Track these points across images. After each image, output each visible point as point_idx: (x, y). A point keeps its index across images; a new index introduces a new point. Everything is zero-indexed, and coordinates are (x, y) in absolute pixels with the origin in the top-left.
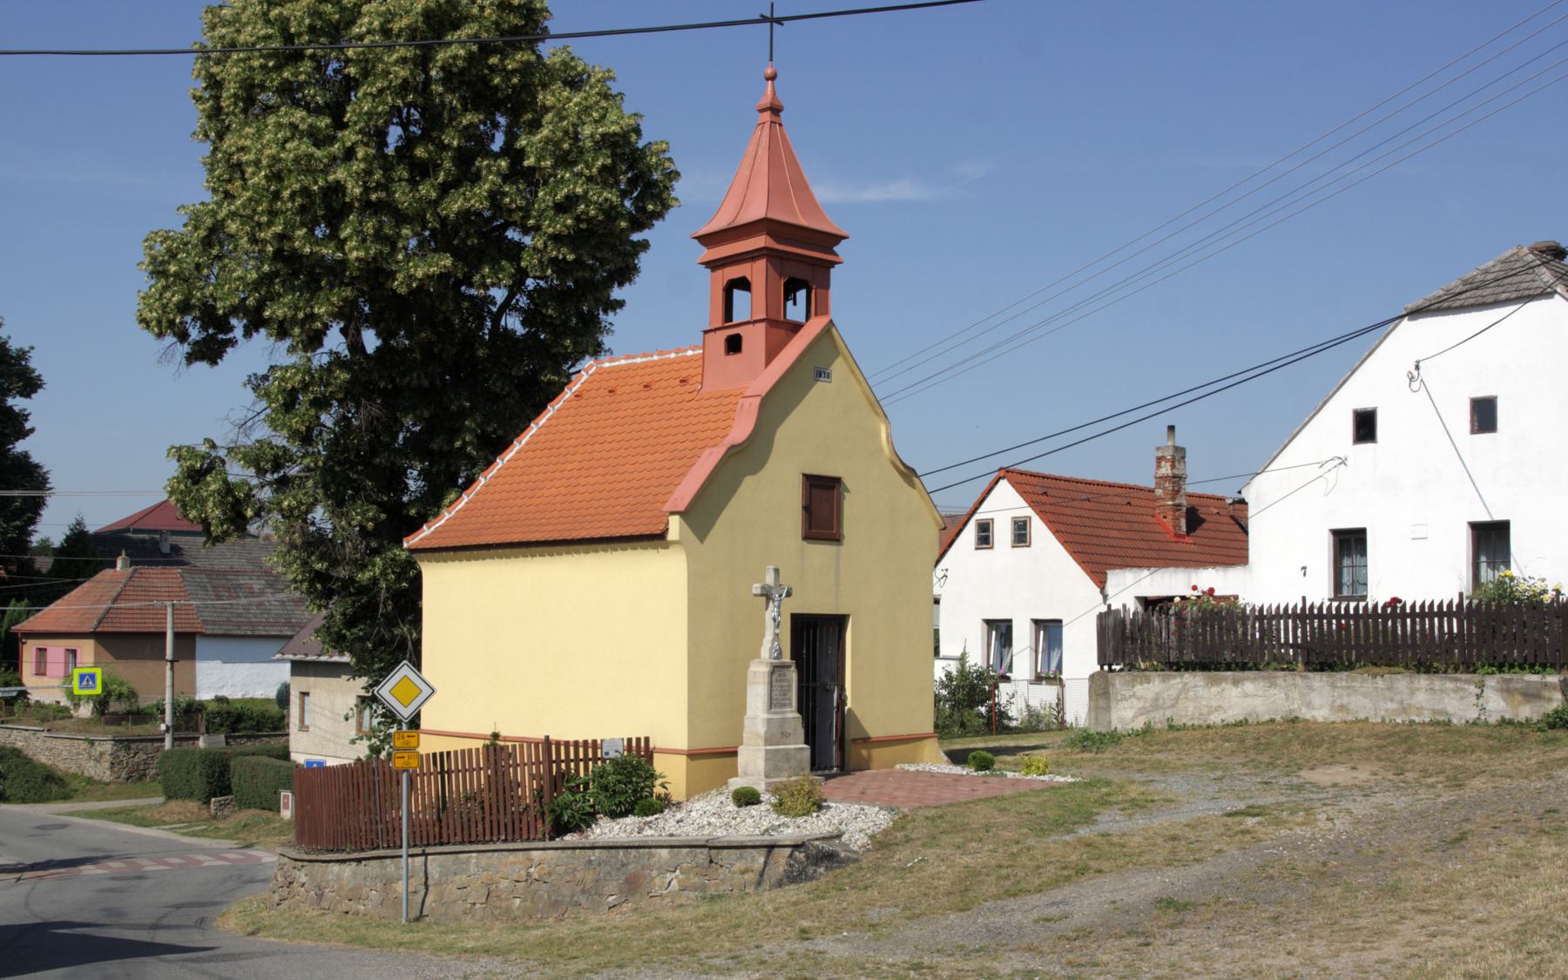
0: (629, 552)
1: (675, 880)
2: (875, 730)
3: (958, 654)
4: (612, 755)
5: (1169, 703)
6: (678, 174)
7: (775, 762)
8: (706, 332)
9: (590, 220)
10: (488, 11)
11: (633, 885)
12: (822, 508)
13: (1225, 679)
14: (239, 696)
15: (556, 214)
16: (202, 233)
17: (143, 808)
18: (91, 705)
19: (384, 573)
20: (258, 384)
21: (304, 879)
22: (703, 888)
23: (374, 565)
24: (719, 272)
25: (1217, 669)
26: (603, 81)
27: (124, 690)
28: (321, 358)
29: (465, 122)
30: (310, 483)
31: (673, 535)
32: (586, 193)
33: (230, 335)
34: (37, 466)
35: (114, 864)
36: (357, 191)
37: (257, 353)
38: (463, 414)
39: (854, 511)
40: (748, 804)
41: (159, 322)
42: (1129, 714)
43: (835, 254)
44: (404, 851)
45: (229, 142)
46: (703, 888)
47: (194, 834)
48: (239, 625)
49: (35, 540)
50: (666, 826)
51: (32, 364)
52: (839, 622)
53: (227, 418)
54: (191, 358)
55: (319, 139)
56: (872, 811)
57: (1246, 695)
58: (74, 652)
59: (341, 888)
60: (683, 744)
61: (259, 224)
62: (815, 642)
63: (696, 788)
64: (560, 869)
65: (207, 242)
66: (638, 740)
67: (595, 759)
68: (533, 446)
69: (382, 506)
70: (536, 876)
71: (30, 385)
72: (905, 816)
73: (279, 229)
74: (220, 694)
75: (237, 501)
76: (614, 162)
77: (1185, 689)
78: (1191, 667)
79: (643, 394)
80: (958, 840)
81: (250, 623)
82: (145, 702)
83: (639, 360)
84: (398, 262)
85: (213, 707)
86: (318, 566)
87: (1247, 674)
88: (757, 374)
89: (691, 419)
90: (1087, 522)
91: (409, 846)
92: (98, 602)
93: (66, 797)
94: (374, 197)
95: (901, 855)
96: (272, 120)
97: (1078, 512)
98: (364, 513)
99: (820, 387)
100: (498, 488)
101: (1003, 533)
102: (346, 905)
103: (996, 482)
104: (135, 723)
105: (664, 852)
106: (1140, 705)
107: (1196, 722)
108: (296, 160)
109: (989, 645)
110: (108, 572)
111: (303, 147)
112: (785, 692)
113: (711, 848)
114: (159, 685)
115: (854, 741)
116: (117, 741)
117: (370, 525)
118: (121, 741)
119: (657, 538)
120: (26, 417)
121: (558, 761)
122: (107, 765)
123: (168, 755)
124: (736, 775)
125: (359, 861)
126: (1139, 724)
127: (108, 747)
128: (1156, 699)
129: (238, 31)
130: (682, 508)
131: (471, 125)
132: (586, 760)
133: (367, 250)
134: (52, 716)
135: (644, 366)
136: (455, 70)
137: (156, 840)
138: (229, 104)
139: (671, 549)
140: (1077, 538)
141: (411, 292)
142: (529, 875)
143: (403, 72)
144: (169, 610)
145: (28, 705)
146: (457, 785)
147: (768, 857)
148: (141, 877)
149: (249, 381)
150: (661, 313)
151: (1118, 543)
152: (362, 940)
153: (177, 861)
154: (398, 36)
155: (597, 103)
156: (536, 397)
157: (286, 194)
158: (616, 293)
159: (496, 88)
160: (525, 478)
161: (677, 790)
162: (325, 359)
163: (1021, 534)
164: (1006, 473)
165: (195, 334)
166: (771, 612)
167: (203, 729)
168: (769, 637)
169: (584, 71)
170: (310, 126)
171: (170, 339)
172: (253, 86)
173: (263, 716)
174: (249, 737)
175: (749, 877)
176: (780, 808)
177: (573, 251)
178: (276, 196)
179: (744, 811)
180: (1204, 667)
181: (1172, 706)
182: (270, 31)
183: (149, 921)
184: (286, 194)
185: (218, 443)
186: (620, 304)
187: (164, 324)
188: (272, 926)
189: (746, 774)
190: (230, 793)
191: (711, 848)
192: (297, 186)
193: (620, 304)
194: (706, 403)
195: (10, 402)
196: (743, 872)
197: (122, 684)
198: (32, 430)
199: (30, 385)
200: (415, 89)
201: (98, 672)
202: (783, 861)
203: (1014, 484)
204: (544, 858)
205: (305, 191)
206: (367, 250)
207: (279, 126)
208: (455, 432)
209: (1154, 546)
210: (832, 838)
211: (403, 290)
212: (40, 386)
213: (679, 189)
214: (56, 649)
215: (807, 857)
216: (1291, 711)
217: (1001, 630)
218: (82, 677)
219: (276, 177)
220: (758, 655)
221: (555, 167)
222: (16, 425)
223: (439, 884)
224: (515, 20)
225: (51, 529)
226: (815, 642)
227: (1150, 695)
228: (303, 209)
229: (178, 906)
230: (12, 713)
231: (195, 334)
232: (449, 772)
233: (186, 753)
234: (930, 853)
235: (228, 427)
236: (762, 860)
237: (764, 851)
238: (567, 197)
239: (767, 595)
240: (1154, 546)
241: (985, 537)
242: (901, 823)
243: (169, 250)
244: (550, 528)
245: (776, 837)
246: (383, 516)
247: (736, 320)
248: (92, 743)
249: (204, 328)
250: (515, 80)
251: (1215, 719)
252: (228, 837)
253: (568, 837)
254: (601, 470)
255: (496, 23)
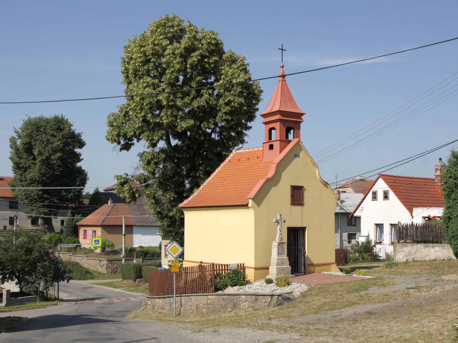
0: (239, 209)
1: (246, 304)
2: (315, 261)
3: (367, 235)
4: (233, 268)
5: (413, 253)
6: (262, 91)
7: (279, 271)
8: (264, 143)
9: (235, 107)
10: (204, 46)
11: (235, 306)
12: (297, 195)
13: (430, 246)
14: (147, 246)
15: (225, 106)
16: (124, 113)
17: (116, 282)
18: (100, 249)
19: (176, 213)
20: (141, 155)
21: (150, 303)
22: (254, 307)
23: (173, 210)
24: (267, 125)
25: (429, 243)
26: (242, 60)
27: (110, 244)
28: (157, 149)
29: (198, 80)
30: (155, 185)
31: (250, 205)
32: (234, 100)
33: (132, 142)
34: (84, 171)
35: (105, 300)
36: (165, 103)
37: (141, 146)
38: (200, 165)
39: (307, 196)
40: (269, 283)
41: (112, 139)
42: (401, 257)
43: (302, 119)
44: (174, 296)
45: (131, 86)
46: (254, 307)
47: (131, 291)
48: (147, 222)
49: (84, 194)
50: (246, 289)
51: (82, 138)
52: (304, 229)
53: (132, 166)
54: (121, 149)
55: (155, 86)
56: (303, 285)
57: (436, 251)
58: (95, 231)
59: (159, 306)
60: (253, 266)
61: (138, 112)
62: (295, 236)
63: (257, 278)
64: (216, 301)
65: (125, 116)
66: (241, 264)
67: (228, 270)
68: (216, 177)
69: (176, 193)
70: (209, 303)
71: (82, 144)
72: (312, 287)
73: (143, 114)
74: (141, 245)
75: (134, 192)
76: (242, 90)
77: (418, 249)
78: (418, 242)
79: (247, 161)
80: (325, 294)
81: (151, 222)
82: (116, 248)
83: (247, 150)
84: (178, 123)
85: (138, 250)
86: (158, 210)
87: (437, 244)
88: (277, 156)
89: (259, 170)
90: (409, 191)
91: (176, 294)
92: (102, 215)
93: (92, 278)
94: (170, 104)
95: (308, 299)
96: (142, 80)
97: (406, 188)
98: (170, 195)
99: (296, 159)
100: (206, 189)
101: (380, 195)
102: (160, 311)
103: (378, 179)
104: (114, 255)
105: (244, 296)
106: (405, 254)
107: (421, 260)
108: (148, 94)
109: (377, 232)
110: (106, 205)
111: (150, 90)
112: (283, 251)
113: (256, 295)
114: (121, 242)
115: (308, 265)
116: (108, 260)
117: (172, 199)
118: (109, 260)
119: (245, 206)
120: (80, 155)
121: (216, 270)
122: (105, 268)
123: (123, 265)
124: (269, 275)
125: (164, 298)
126: (404, 260)
127: (105, 262)
128: (409, 252)
129: (133, 54)
130: (252, 197)
131: (199, 80)
132: (225, 270)
133: (168, 120)
134: (89, 252)
135: (248, 152)
136: (194, 65)
137: (119, 293)
138: (132, 75)
139: (250, 209)
140: (405, 197)
141: (182, 131)
142: (208, 302)
143: (178, 66)
144: (123, 218)
145: (81, 249)
146: (190, 278)
147: (271, 298)
148: (112, 304)
149: (233, 54)
150: (256, 133)
151: (421, 198)
152: (161, 320)
153: (124, 299)
154: (177, 55)
155: (237, 72)
156: (221, 158)
157: (145, 104)
158: (249, 124)
159: (207, 68)
160: (213, 186)
161: (252, 280)
162: (158, 150)
163: (386, 197)
164: (381, 176)
165: (122, 142)
166: (279, 227)
167: (135, 257)
168: (278, 234)
169: (237, 57)
170: (152, 82)
171: (115, 144)
172: (136, 71)
173: (154, 253)
174: (150, 259)
175: (266, 304)
176: (277, 284)
177: (230, 117)
178: (143, 104)
179: (268, 285)
180: (425, 242)
181: (414, 254)
182: (141, 55)
183: (108, 315)
184: (145, 104)
185: (129, 174)
186: (250, 127)
187: (113, 140)
188: (140, 316)
189: (271, 274)
190: (142, 278)
191: (256, 295)
192: (148, 102)
193: (250, 127)
194: (263, 165)
195: (76, 150)
196: (265, 303)
197: (109, 242)
198: (82, 159)
199: (82, 144)
200: (182, 71)
201: (100, 239)
202: (275, 300)
203: (384, 179)
204: (212, 298)
205: (150, 103)
206: (168, 120)
207: (144, 82)
208: (197, 170)
209: (433, 199)
210: (290, 293)
211: (180, 131)
212: (85, 145)
213: (263, 96)
214: (90, 230)
215: (282, 298)
216: (450, 256)
217: (379, 226)
218: (95, 241)
219: (143, 99)
220: (275, 240)
221: (224, 92)
222: (77, 158)
223: (184, 305)
224: (212, 47)
225: (89, 189)
226: (295, 236)
227: (408, 251)
228: (150, 108)
229: (119, 312)
230: (76, 251)
231: (122, 142)
232: (188, 273)
233: (129, 265)
234: (315, 298)
235: (132, 169)
236: (270, 299)
237: (270, 297)
238: (228, 101)
239: (277, 222)
240: (433, 199)
241: (375, 197)
242: (309, 290)
243: (114, 118)
244: (218, 202)
245: (275, 293)
246: (176, 196)
247: (273, 140)
248: (100, 261)
249: (125, 140)
250: (212, 66)
251: (427, 259)
252: (141, 292)
253: (219, 292)
254: (234, 185)
255: (207, 49)
